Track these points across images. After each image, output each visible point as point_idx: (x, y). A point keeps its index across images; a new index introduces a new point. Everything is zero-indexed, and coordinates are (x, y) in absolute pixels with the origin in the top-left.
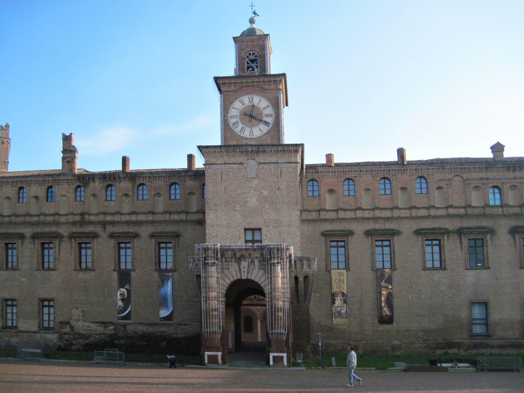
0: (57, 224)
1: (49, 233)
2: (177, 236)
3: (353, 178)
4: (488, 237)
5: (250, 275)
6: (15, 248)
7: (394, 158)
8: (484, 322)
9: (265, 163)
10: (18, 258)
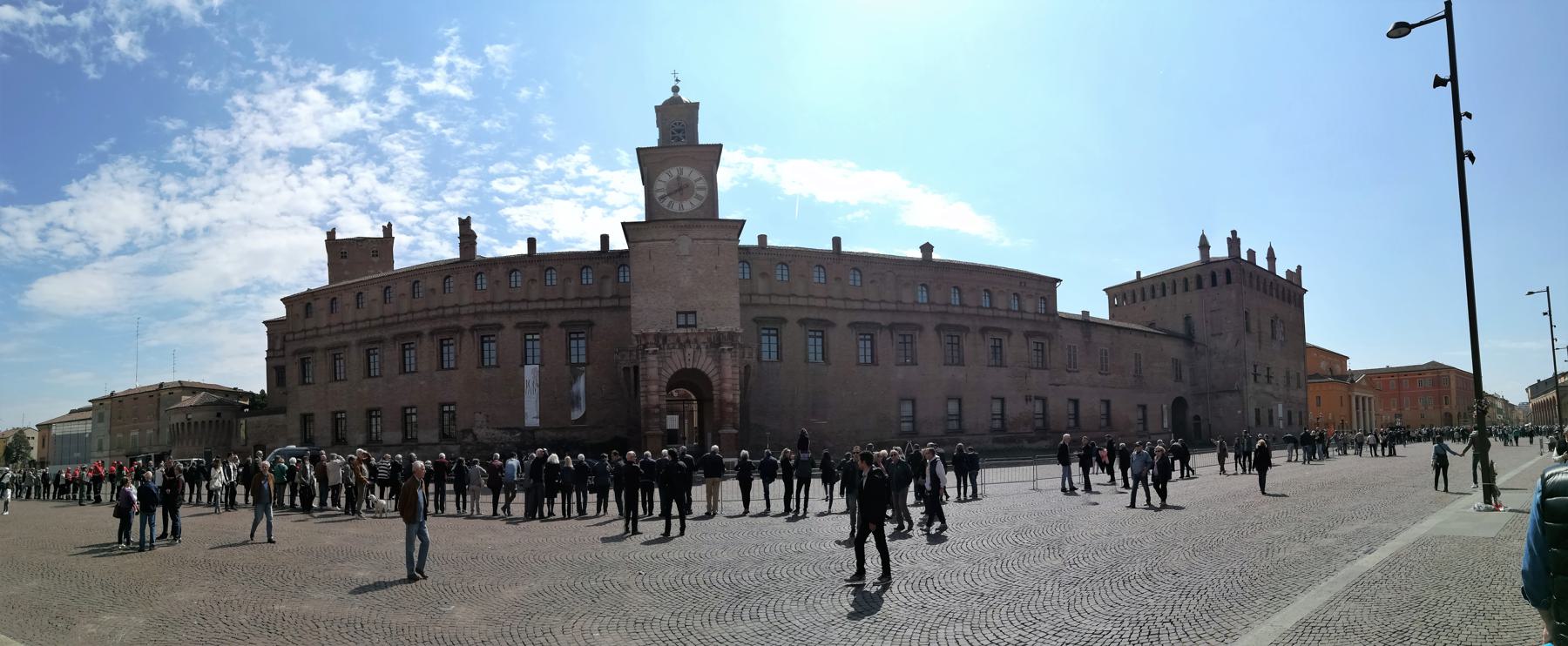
0: (458, 316)
1: (448, 327)
2: (591, 324)
3: (787, 263)
4: (917, 333)
5: (696, 364)
6: (413, 349)
7: (828, 246)
8: (911, 419)
9: (700, 239)
10: (416, 359)
